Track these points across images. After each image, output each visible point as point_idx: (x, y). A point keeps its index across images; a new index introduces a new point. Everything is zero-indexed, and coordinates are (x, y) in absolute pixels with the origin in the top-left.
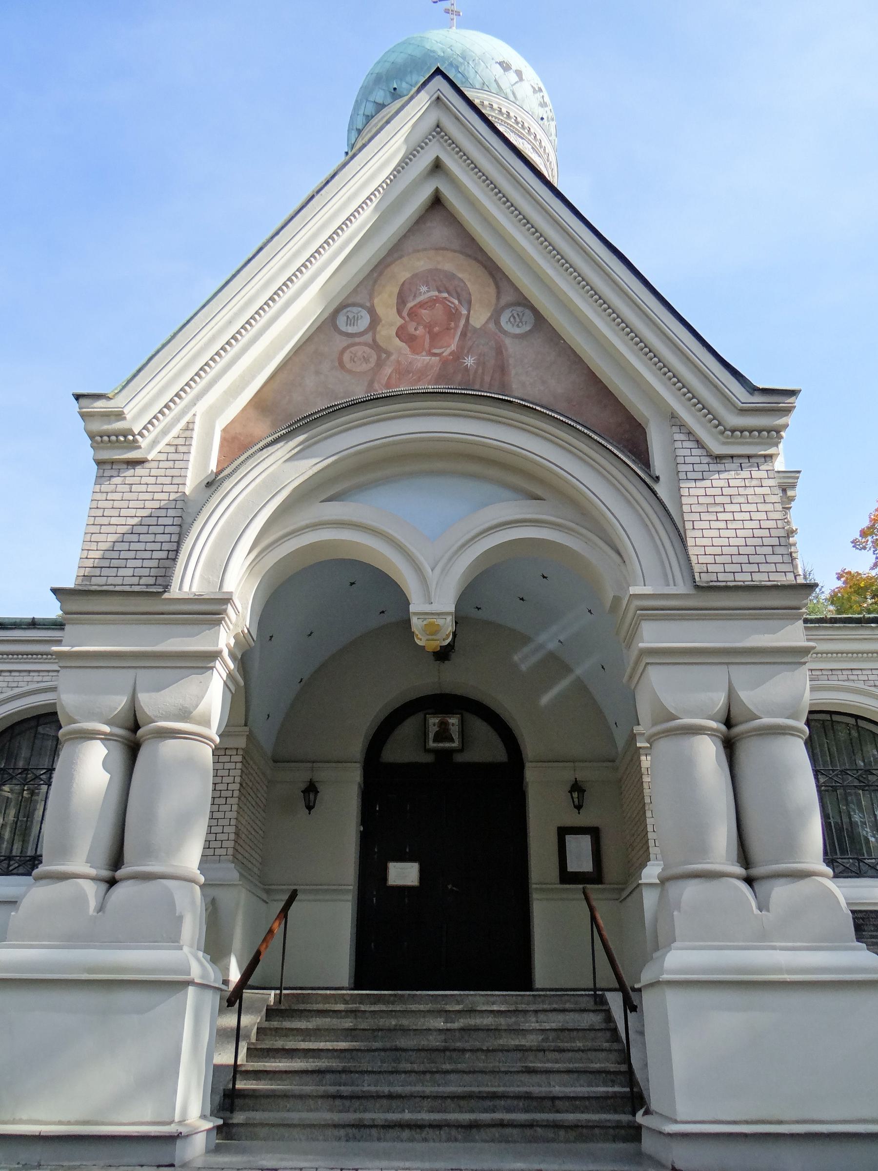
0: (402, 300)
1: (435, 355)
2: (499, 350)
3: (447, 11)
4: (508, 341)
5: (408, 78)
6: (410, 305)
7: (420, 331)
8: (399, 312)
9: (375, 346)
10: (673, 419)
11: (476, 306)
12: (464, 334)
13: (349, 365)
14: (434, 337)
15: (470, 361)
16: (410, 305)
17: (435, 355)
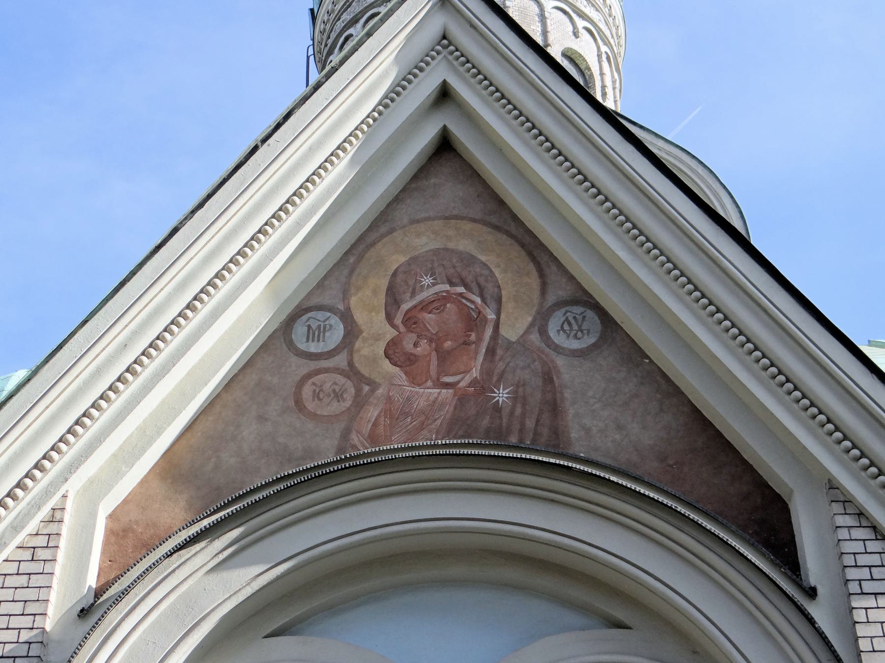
1: (447, 385)
2: (548, 377)
4: (560, 361)
6: (405, 307)
7: (423, 348)
8: (390, 318)
9: (352, 372)
11: (508, 306)
12: (491, 352)
13: (310, 406)
14: (444, 357)
15: (502, 395)
16: (405, 307)
17: (447, 385)
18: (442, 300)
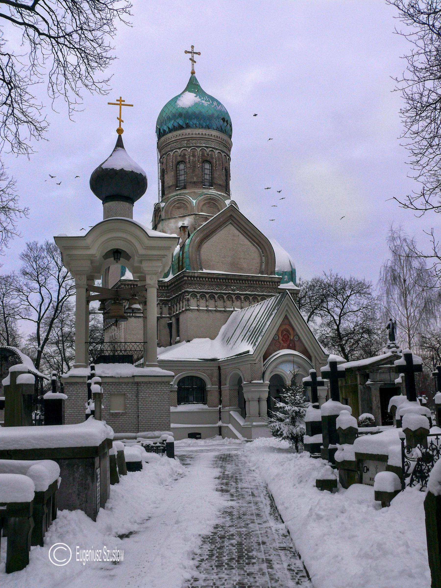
0: (282, 335)
3: (190, 59)
5: (193, 121)
10: (315, 357)
15: (291, 345)
18: (286, 334)
